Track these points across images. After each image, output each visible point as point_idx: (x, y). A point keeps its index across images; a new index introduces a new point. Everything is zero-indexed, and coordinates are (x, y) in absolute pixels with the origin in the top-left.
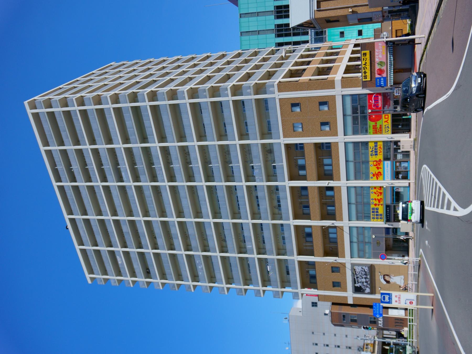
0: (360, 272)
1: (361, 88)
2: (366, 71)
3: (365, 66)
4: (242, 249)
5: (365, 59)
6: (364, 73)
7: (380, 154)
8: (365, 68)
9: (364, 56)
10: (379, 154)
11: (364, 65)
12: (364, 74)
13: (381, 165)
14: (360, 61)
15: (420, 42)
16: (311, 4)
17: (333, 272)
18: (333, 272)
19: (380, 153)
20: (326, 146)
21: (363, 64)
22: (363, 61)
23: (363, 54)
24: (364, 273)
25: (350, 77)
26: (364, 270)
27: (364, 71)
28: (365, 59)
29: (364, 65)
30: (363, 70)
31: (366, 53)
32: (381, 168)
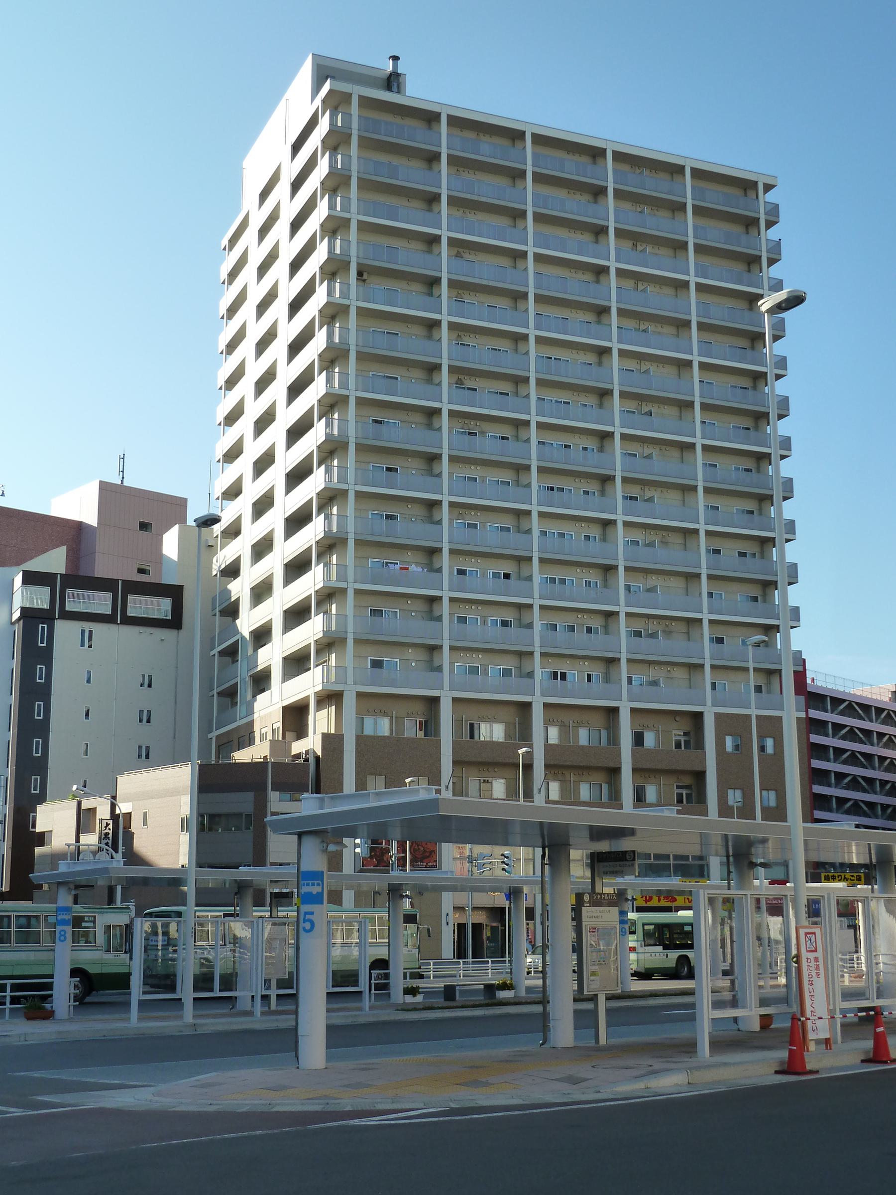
0: (420, 847)
1: (443, 1000)
2: (836, 879)
3: (843, 878)
4: (426, 562)
5: (852, 878)
6: (833, 876)
7: (687, 901)
8: (840, 878)
9: (857, 876)
10: (686, 899)
11: (845, 875)
12: (831, 876)
13: (665, 900)
14: (476, 726)
15: (684, 461)
16: (704, 932)
17: (139, 746)
18: (139, 746)
19: (687, 900)
20: (682, 793)
21: (846, 874)
22: (851, 876)
23: (859, 876)
24: (418, 856)
25: (863, 921)
26: (428, 857)
27: (835, 876)
28: (852, 878)
29: (845, 875)
30: (836, 875)
31: (861, 881)
32: (659, 901)
